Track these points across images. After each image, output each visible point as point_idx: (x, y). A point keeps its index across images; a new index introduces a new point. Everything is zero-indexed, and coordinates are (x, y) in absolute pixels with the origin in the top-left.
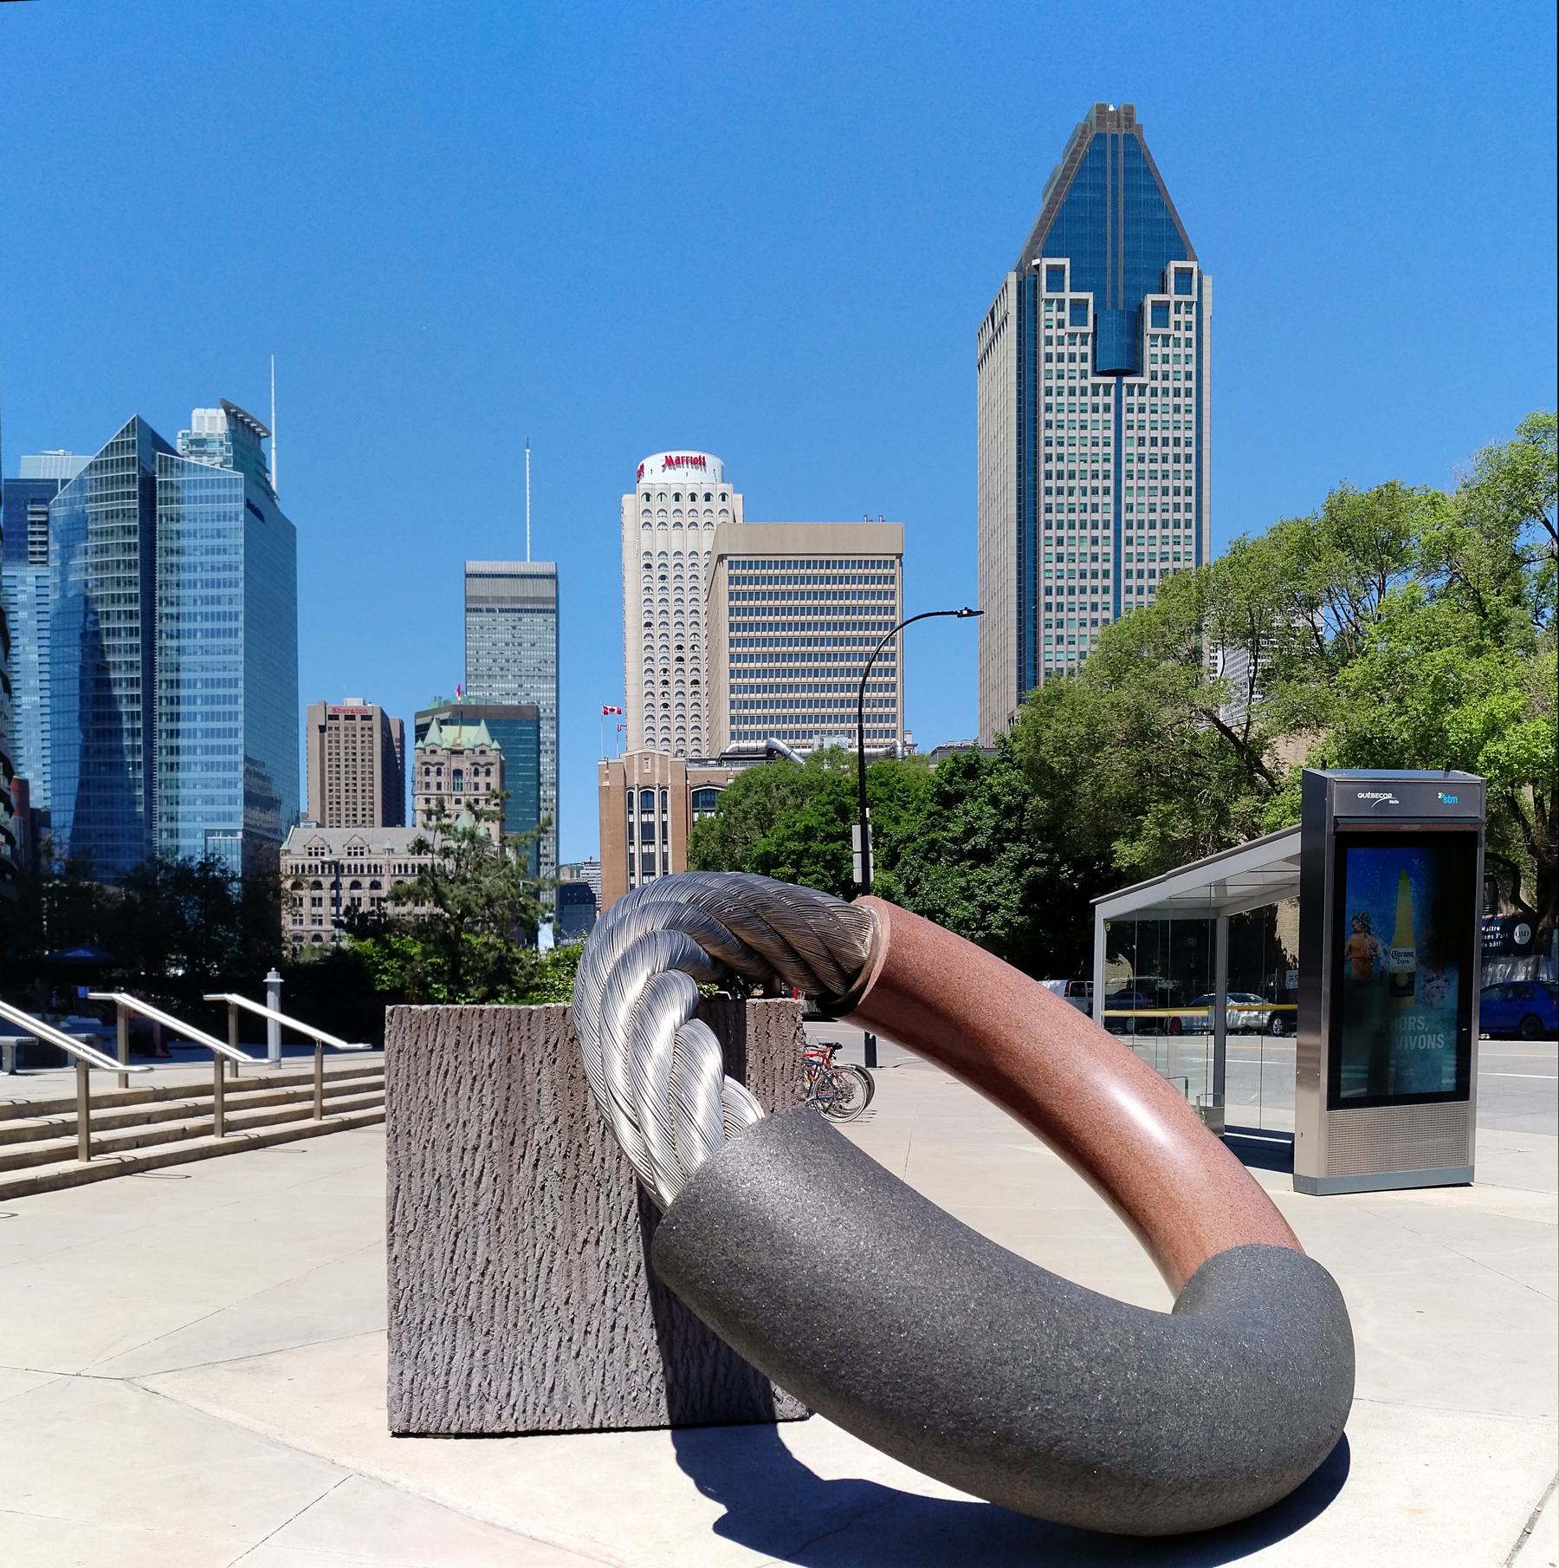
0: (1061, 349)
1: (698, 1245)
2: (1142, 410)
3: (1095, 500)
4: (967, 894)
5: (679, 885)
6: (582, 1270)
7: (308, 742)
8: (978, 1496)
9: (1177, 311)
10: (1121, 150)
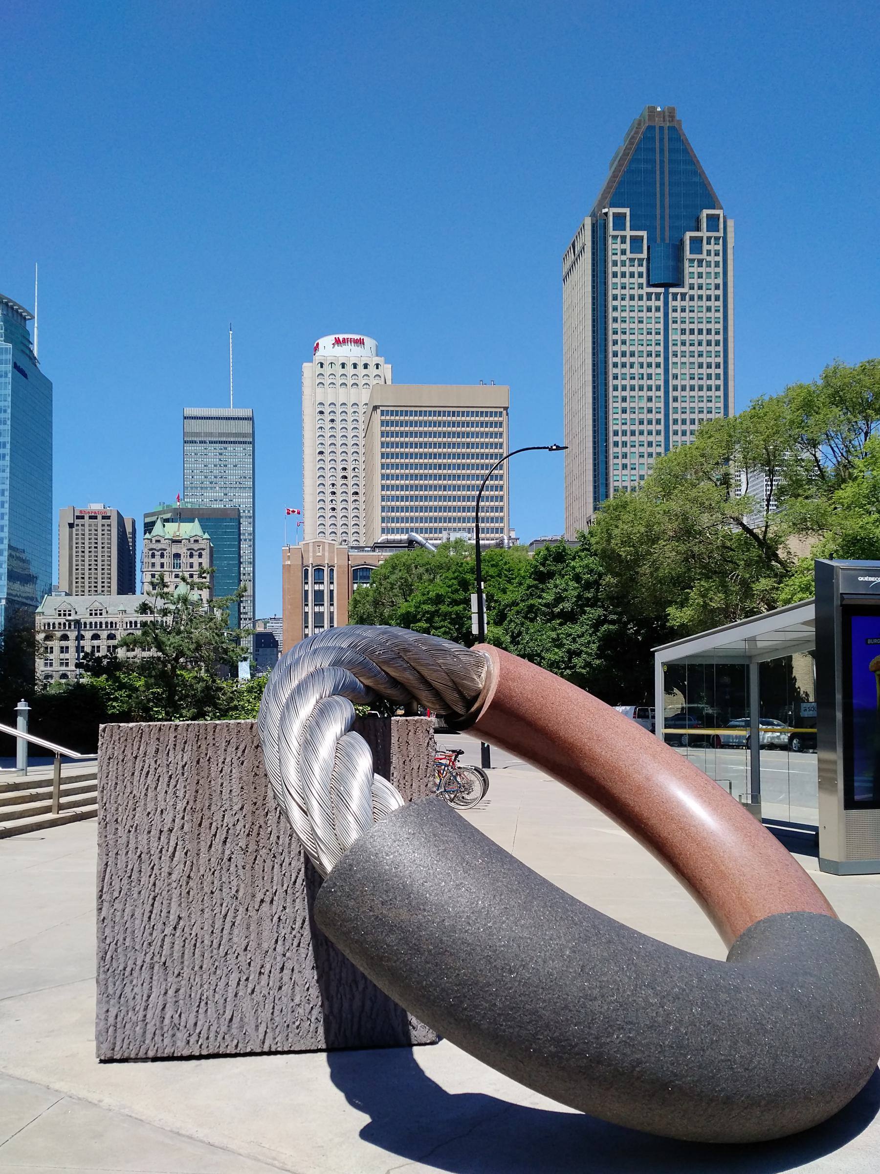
0: (623, 269)
1: (352, 903)
2: (683, 310)
3: (650, 371)
4: (557, 643)
5: (341, 635)
6: (259, 924)
7: (60, 536)
8: (576, 1108)
9: (709, 243)
10: (666, 137)
